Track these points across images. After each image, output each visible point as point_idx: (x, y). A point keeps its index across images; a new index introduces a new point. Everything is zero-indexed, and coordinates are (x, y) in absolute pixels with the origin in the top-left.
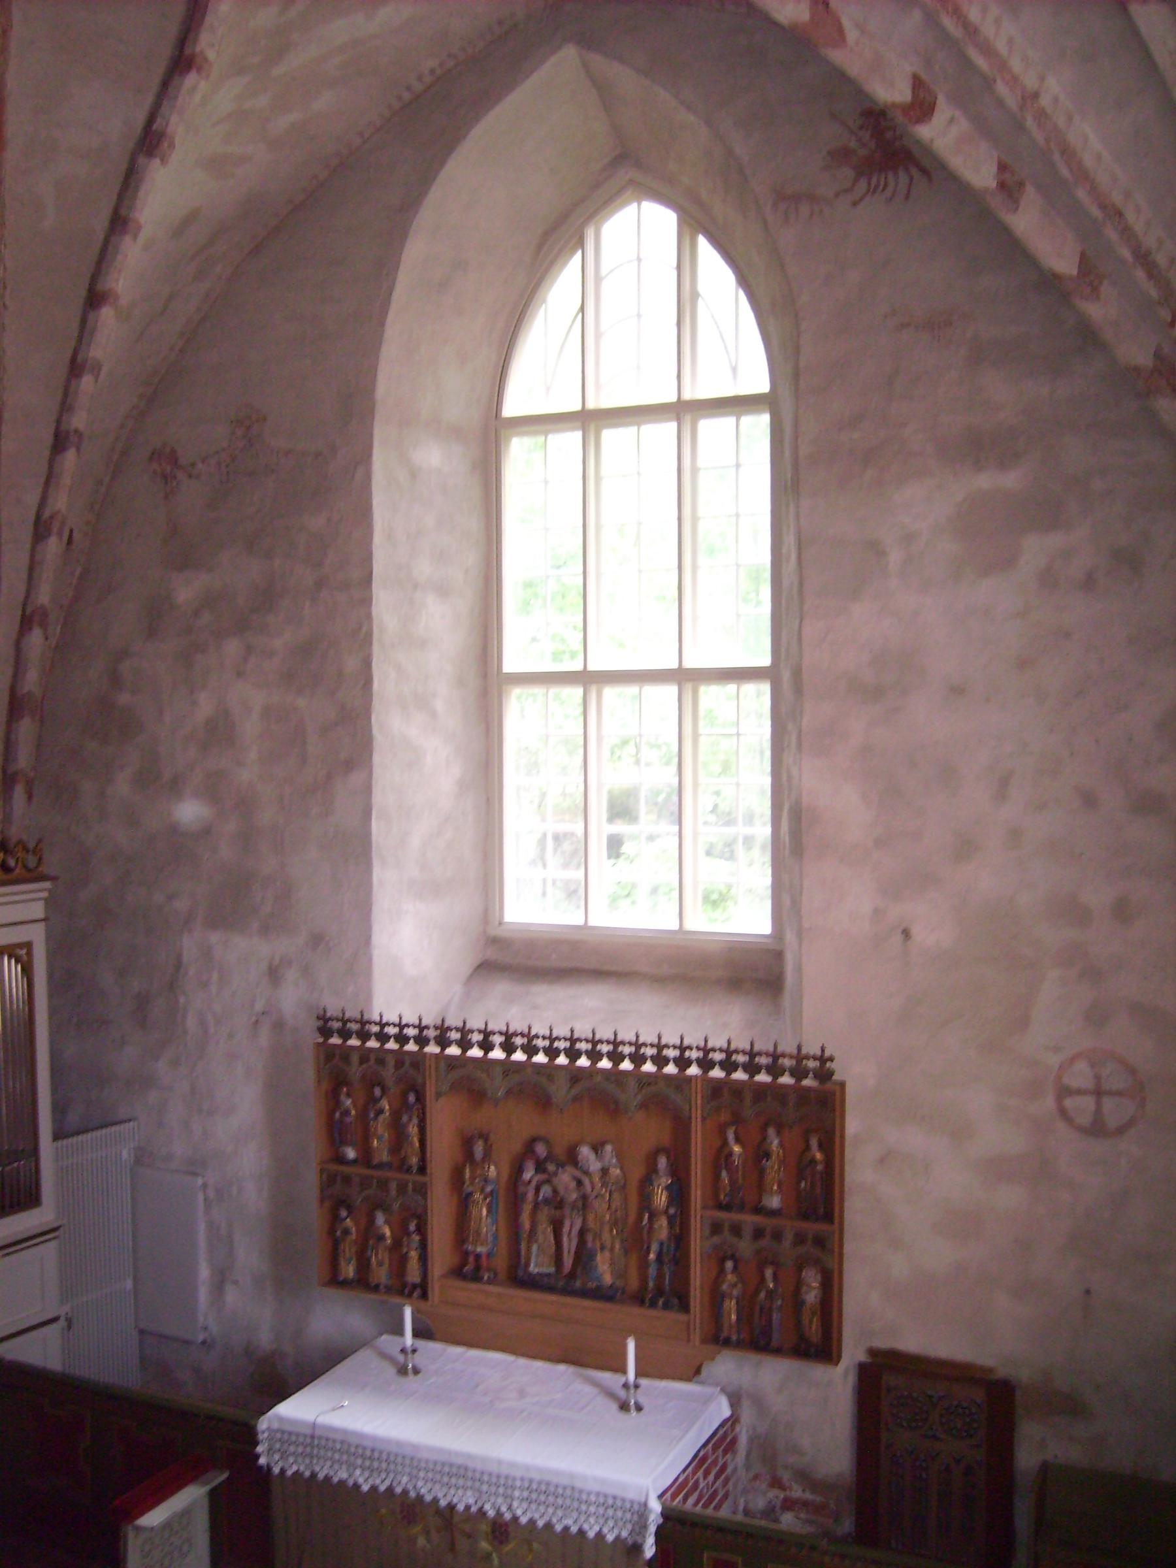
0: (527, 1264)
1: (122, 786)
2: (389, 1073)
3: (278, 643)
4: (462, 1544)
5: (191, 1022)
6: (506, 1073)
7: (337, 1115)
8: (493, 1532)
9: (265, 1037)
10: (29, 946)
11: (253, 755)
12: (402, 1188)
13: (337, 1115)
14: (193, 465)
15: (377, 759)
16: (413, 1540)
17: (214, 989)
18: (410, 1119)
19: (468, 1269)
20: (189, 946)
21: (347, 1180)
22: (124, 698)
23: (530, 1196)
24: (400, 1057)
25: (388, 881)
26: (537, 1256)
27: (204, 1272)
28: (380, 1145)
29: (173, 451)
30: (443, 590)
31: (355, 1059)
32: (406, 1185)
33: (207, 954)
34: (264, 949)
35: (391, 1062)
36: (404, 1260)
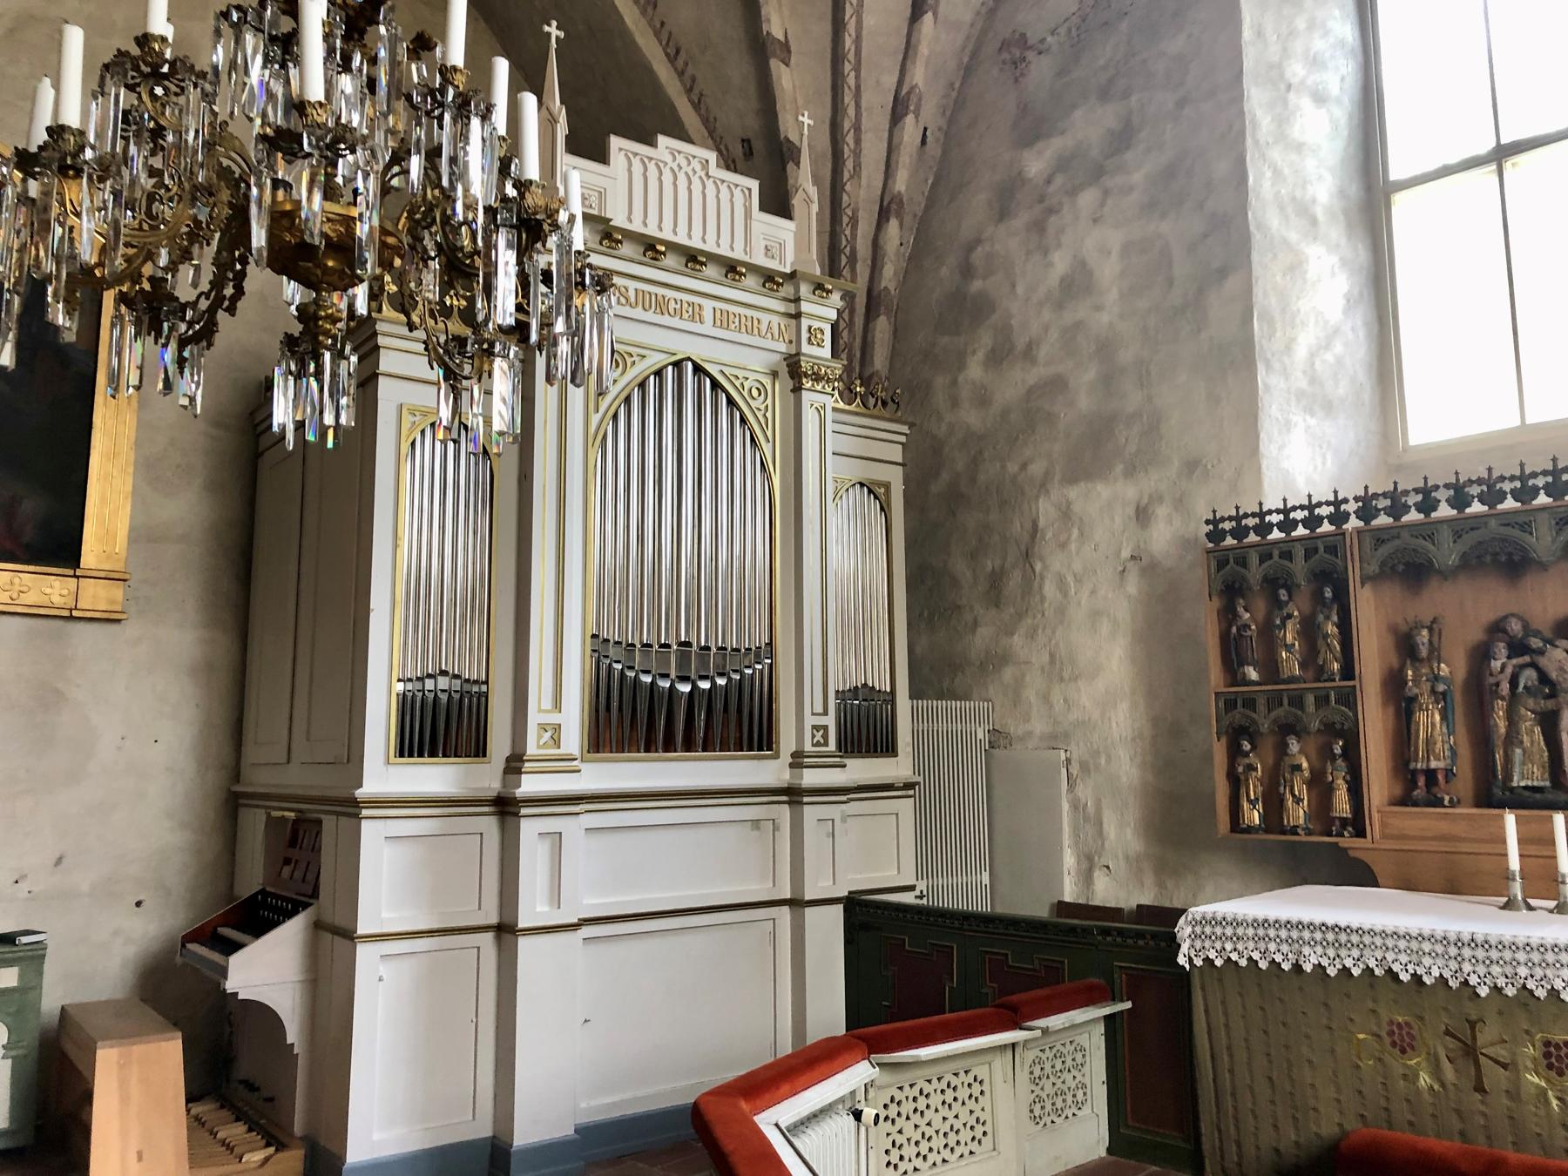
0: (1508, 776)
1: (975, 370)
2: (1299, 567)
3: (1137, 177)
4: (1495, 1077)
5: (1050, 589)
6: (1458, 535)
7: (1234, 630)
8: (1547, 1055)
9: (1133, 586)
10: (887, 486)
11: (1113, 295)
12: (1322, 701)
13: (1234, 630)
14: (1043, 41)
15: (1255, 257)
16: (1410, 1077)
17: (1073, 546)
18: (1328, 618)
19: (1418, 786)
20: (1046, 510)
21: (1250, 703)
22: (976, 285)
23: (1505, 688)
24: (1310, 547)
25: (1277, 391)
26: (1523, 763)
27: (1069, 860)
28: (1291, 663)
29: (1023, 35)
30: (1320, 98)
31: (1254, 559)
32: (1327, 697)
33: (1066, 514)
34: (1129, 492)
35: (1299, 552)
36: (1329, 790)
